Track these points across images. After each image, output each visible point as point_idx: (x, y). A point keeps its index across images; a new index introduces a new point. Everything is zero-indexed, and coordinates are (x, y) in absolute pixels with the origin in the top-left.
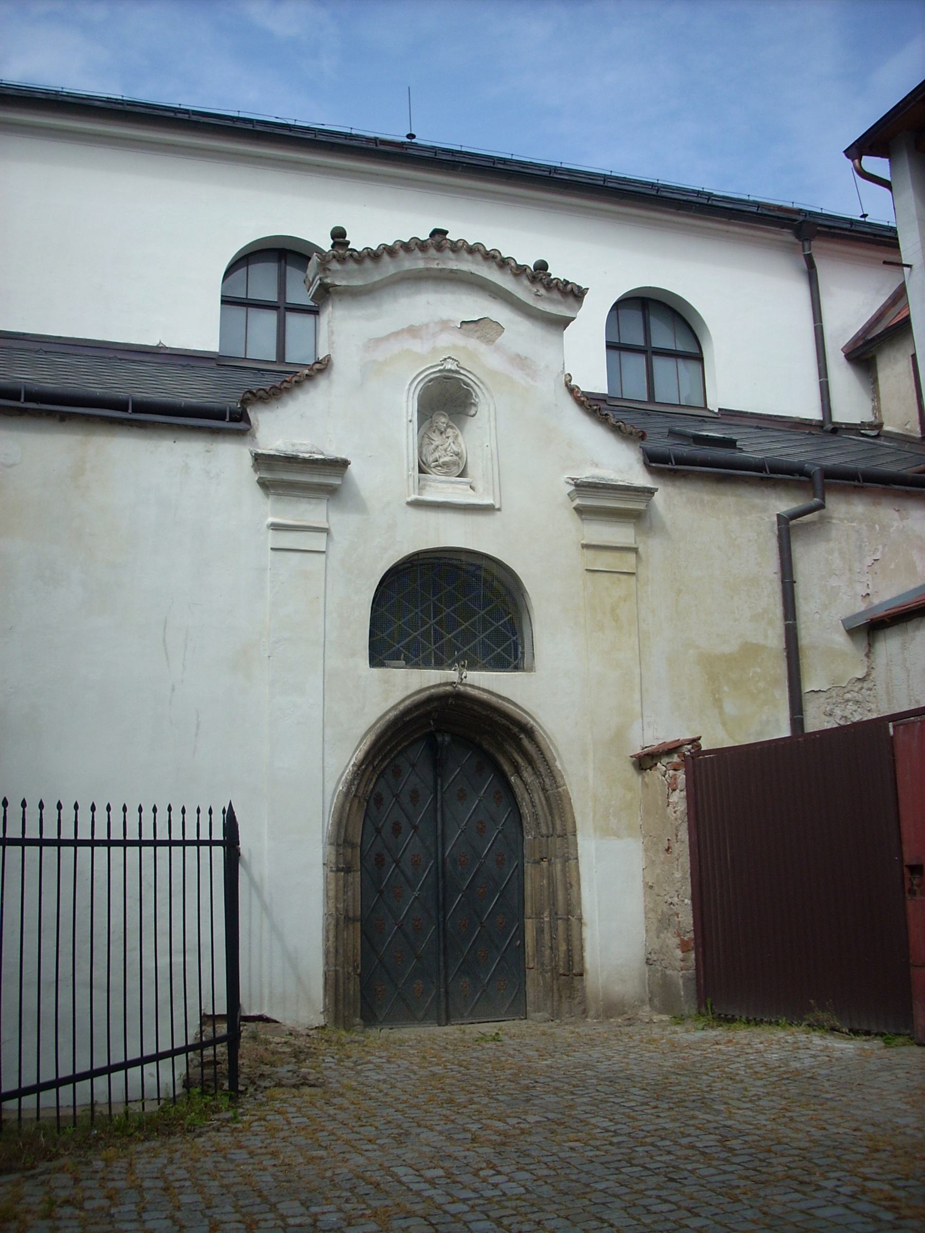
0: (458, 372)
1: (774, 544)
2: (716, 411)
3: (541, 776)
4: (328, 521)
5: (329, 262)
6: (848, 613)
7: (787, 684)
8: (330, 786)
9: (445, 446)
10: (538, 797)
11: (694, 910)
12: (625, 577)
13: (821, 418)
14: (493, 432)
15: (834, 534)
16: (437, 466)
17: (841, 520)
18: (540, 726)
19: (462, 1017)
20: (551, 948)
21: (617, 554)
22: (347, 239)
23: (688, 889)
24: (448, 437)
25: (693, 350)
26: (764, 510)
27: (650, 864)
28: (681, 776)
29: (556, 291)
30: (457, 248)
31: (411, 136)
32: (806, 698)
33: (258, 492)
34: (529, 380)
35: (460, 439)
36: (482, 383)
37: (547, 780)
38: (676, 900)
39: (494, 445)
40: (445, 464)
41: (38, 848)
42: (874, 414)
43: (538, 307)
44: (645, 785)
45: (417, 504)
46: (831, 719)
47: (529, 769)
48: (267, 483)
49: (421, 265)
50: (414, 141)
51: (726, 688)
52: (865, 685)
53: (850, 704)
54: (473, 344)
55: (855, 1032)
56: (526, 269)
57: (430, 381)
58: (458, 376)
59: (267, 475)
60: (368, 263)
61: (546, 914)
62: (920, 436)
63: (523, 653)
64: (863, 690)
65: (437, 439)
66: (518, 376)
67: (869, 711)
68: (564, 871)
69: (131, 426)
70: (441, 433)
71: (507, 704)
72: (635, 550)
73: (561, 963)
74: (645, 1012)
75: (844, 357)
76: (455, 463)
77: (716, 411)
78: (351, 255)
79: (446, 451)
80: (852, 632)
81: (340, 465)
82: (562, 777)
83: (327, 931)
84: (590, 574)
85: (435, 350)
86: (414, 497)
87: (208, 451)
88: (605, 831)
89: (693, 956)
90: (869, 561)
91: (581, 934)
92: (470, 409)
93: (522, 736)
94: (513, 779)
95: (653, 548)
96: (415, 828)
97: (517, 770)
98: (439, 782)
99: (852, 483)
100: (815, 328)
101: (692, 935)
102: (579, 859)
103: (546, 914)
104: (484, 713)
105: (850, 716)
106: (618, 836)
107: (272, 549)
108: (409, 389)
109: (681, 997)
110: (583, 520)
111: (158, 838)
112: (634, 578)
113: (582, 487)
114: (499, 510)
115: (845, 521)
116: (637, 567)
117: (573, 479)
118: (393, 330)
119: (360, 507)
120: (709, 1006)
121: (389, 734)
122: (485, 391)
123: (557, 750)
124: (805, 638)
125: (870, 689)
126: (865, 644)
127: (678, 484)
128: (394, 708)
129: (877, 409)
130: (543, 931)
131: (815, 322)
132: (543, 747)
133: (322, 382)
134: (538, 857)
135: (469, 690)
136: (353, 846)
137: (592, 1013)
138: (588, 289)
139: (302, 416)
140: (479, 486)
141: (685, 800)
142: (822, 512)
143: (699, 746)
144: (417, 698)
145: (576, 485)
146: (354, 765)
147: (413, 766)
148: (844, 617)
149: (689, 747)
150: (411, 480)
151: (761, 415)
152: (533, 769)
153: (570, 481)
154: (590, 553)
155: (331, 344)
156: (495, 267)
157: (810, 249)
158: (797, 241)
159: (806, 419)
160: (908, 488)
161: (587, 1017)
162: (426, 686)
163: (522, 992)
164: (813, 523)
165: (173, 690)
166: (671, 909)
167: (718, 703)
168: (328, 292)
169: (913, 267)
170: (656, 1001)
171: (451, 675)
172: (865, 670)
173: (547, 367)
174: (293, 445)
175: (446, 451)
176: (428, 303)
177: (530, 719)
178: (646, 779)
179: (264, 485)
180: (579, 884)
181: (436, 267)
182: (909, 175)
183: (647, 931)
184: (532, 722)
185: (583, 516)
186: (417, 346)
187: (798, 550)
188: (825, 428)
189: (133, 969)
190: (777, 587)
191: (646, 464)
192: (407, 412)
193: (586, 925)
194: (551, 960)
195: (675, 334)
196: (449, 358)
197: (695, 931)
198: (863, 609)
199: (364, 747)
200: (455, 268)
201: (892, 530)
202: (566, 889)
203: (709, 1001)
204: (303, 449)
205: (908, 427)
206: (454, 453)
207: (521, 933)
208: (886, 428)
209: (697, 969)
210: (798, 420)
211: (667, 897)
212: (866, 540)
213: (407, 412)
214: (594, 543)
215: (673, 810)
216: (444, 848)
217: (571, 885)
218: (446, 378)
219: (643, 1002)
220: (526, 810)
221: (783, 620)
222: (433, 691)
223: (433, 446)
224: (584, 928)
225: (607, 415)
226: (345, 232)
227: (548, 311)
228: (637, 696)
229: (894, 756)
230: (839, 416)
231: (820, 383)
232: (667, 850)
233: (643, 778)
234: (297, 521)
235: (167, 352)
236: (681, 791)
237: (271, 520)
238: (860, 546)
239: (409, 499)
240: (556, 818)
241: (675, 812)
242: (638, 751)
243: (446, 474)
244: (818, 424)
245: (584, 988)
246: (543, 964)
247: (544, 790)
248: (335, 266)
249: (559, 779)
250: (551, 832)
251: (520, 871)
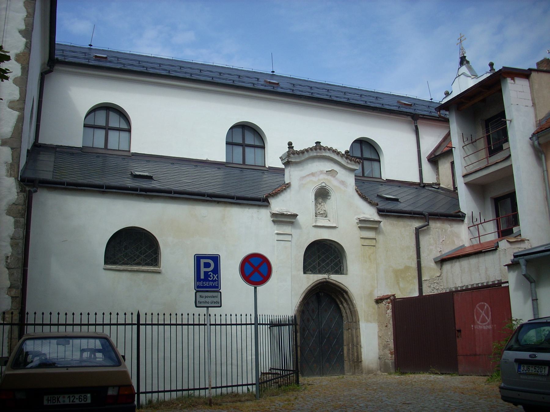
0: (326, 187)
1: (414, 236)
2: (385, 180)
3: (349, 305)
4: (291, 232)
5: (290, 154)
6: (435, 257)
7: (417, 278)
8: (294, 308)
9: (321, 208)
10: (348, 311)
11: (394, 343)
12: (373, 247)
13: (419, 182)
14: (335, 204)
15: (431, 233)
16: (320, 214)
17: (434, 228)
18: (350, 291)
19: (326, 374)
20: (352, 355)
21: (370, 240)
22: (293, 145)
23: (392, 337)
24: (322, 205)
25: (377, 158)
26: (411, 226)
27: (380, 330)
28: (390, 305)
29: (353, 161)
30: (325, 149)
31: (273, 72)
32: (423, 282)
33: (272, 224)
35: (325, 205)
36: (332, 190)
37: (351, 306)
38: (389, 340)
39: (336, 208)
40: (322, 214)
41: (157, 326)
42: (437, 180)
43: (348, 166)
44: (379, 308)
45: (316, 226)
46: (430, 288)
47: (346, 303)
48: (275, 221)
49: (315, 154)
50: (274, 73)
51: (400, 279)
52: (440, 278)
53: (435, 284)
54: (329, 178)
55: (442, 374)
57: (318, 189)
58: (325, 188)
59: (275, 219)
60: (301, 155)
61: (350, 345)
62: (453, 190)
63: (343, 269)
64: (439, 280)
65: (319, 206)
66: (342, 187)
67: (441, 286)
68: (355, 332)
69: (237, 204)
70: (320, 204)
71: (340, 284)
72: (375, 239)
73: (355, 359)
74: (379, 372)
75: (427, 161)
76: (324, 213)
77: (385, 180)
78: (296, 152)
79: (322, 209)
80: (436, 262)
81: (295, 216)
82: (355, 305)
84: (363, 246)
86: (314, 224)
87: (258, 212)
88: (368, 321)
89: (394, 356)
90: (441, 241)
91: (361, 350)
92: (328, 197)
93: (344, 293)
94: (340, 306)
95: (380, 238)
96: (313, 320)
97: (342, 304)
98: (320, 306)
99: (437, 217)
100: (418, 151)
101: (393, 350)
103: (350, 345)
104: (334, 287)
105: (435, 287)
106: (371, 322)
107: (277, 240)
108: (312, 192)
109: (390, 367)
110: (361, 230)
111: (216, 323)
112: (375, 247)
113: (361, 221)
114: (337, 227)
115: (435, 229)
116: (376, 244)
117: (359, 218)
118: (307, 174)
119: (300, 227)
120: (399, 370)
121: (308, 293)
122: (333, 192)
123: (354, 297)
124: (423, 264)
125: (441, 279)
126: (440, 266)
127: (387, 218)
128: (310, 286)
129: (438, 178)
130: (349, 349)
131: (418, 149)
132: (350, 297)
133: (288, 190)
134: (347, 328)
135: (330, 280)
137: (364, 373)
139: (283, 201)
140: (332, 220)
141: (391, 312)
142: (428, 226)
143: (395, 297)
144: (316, 283)
145: (360, 220)
146: (300, 302)
147: (312, 302)
148: (434, 258)
149: (392, 297)
150: (313, 219)
151: (400, 181)
152: (347, 303)
153: (358, 219)
154: (363, 240)
155: (290, 179)
156: (336, 154)
157: (417, 123)
158: (412, 120)
159: (414, 182)
160: (453, 218)
161: (363, 374)
162: (318, 279)
163: (343, 368)
164: (425, 229)
166: (387, 343)
167: (398, 284)
168: (289, 163)
169: (456, 148)
170: (382, 370)
171: (325, 276)
172: (440, 274)
173: (350, 184)
174: (281, 209)
175: (322, 209)
176: (317, 165)
177: (347, 289)
178: (379, 306)
179: (273, 221)
180: (360, 336)
182: (456, 123)
183: (379, 350)
184: (347, 290)
185: (361, 229)
186: (314, 179)
187: (421, 238)
188: (421, 185)
189: (239, 358)
190: (415, 249)
191: (378, 213)
192: (312, 199)
193: (362, 348)
194: (352, 358)
195: (371, 154)
196: (323, 182)
197: (394, 349)
198: (439, 255)
199: (302, 297)
200: (324, 155)
201: (448, 231)
202: (357, 338)
203: (399, 368)
204: (284, 211)
205: (449, 186)
206: (324, 210)
207: (342, 350)
208: (441, 186)
209: (395, 359)
210: (412, 183)
211: (386, 340)
212: (440, 234)
213: (312, 199)
214: (364, 237)
216: (321, 326)
217: (358, 336)
218: (322, 188)
219: (378, 370)
220: (344, 315)
221: (416, 259)
222: (320, 281)
223: (318, 208)
224: (362, 349)
225: (367, 198)
228: (376, 282)
229: (453, 301)
230: (425, 181)
231: (419, 170)
232: (386, 326)
233: (378, 306)
234: (283, 232)
235: (209, 162)
236: (390, 309)
237: (276, 232)
238: (439, 236)
239: (313, 225)
240: (354, 317)
241: (389, 316)
242: (376, 298)
243: (322, 217)
244: (418, 184)
245: (362, 366)
246: (349, 359)
247: (350, 309)
248: (292, 156)
249: (354, 306)
250: (352, 321)
251: (342, 333)
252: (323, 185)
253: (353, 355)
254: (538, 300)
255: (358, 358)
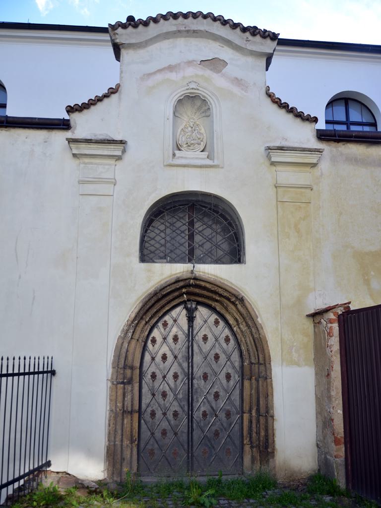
0: (198, 90)
34: (243, 92)
51: (372, 273)
54: (208, 73)
56: (239, 25)
66: (236, 90)
82: (262, 328)
83: (109, 421)
85: (184, 78)
91: (273, 426)
102: (272, 378)
106: (298, 365)
118: (159, 68)
136: (132, 368)
138: (279, 34)
165: (20, 277)
167: (367, 282)
181: (184, 29)
215: (330, 350)
226: (132, 16)
227: (254, 50)
252: (193, 86)
253: (258, 433)
254: (55, 379)
255: (268, 443)
